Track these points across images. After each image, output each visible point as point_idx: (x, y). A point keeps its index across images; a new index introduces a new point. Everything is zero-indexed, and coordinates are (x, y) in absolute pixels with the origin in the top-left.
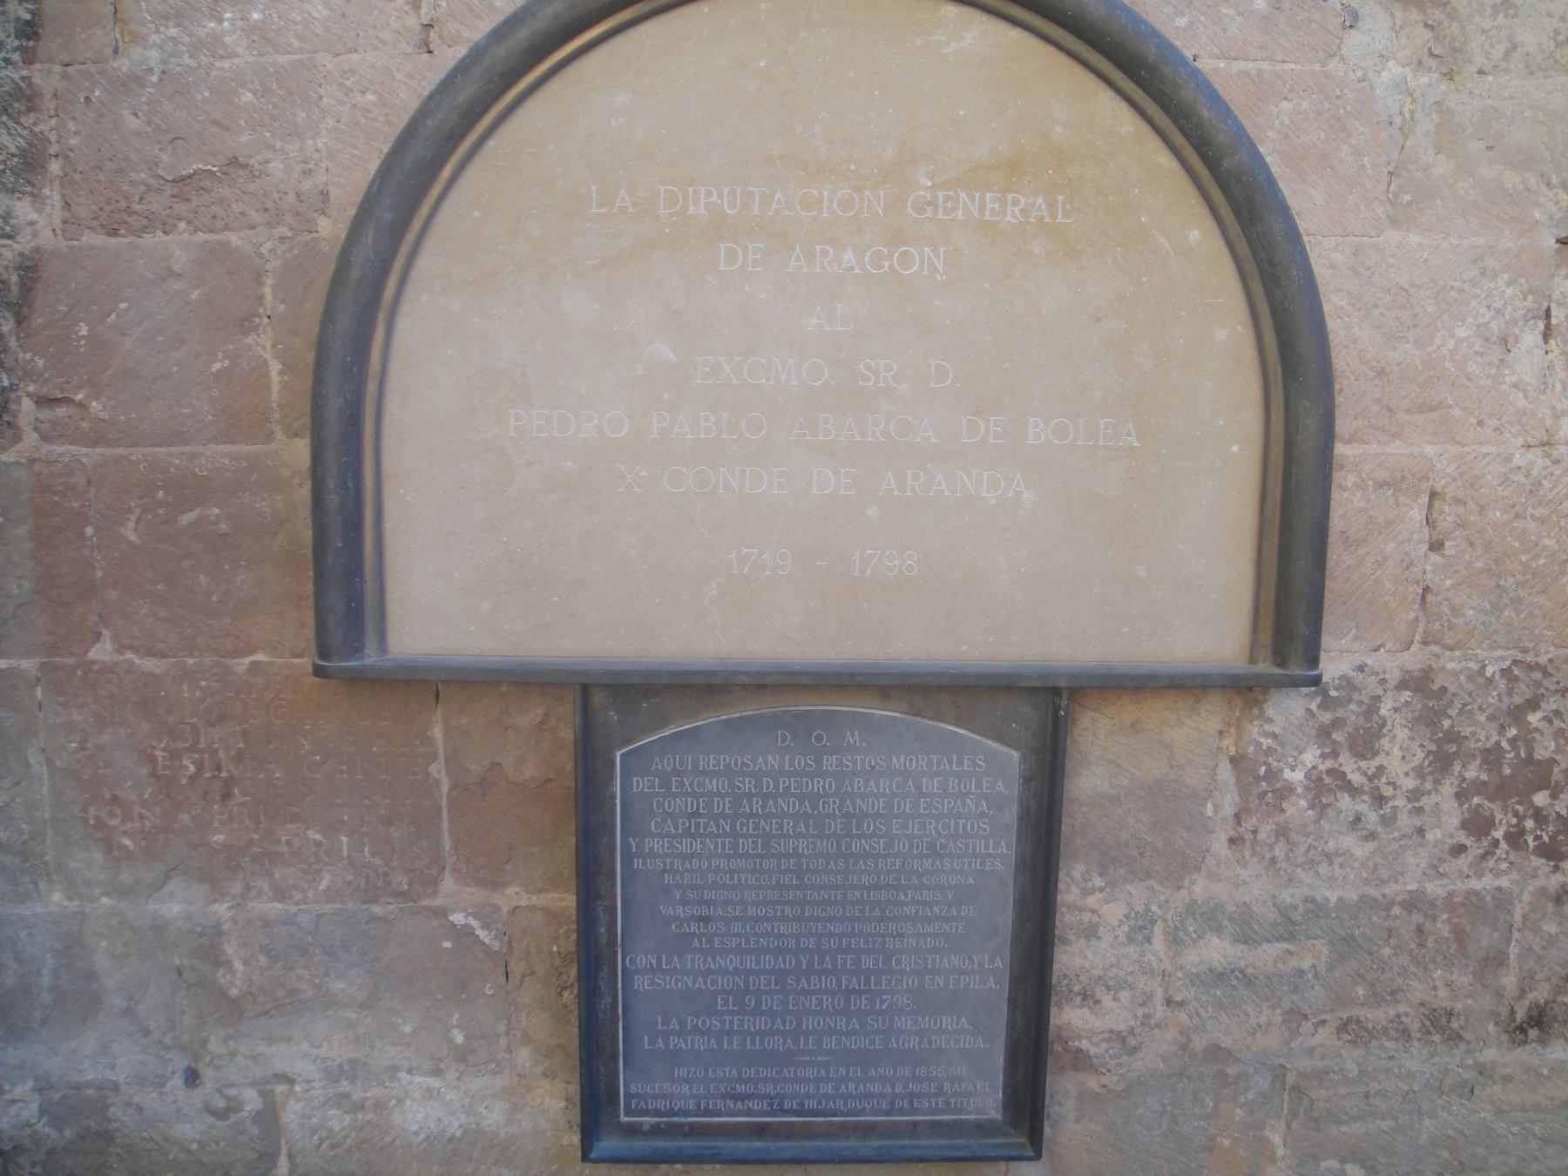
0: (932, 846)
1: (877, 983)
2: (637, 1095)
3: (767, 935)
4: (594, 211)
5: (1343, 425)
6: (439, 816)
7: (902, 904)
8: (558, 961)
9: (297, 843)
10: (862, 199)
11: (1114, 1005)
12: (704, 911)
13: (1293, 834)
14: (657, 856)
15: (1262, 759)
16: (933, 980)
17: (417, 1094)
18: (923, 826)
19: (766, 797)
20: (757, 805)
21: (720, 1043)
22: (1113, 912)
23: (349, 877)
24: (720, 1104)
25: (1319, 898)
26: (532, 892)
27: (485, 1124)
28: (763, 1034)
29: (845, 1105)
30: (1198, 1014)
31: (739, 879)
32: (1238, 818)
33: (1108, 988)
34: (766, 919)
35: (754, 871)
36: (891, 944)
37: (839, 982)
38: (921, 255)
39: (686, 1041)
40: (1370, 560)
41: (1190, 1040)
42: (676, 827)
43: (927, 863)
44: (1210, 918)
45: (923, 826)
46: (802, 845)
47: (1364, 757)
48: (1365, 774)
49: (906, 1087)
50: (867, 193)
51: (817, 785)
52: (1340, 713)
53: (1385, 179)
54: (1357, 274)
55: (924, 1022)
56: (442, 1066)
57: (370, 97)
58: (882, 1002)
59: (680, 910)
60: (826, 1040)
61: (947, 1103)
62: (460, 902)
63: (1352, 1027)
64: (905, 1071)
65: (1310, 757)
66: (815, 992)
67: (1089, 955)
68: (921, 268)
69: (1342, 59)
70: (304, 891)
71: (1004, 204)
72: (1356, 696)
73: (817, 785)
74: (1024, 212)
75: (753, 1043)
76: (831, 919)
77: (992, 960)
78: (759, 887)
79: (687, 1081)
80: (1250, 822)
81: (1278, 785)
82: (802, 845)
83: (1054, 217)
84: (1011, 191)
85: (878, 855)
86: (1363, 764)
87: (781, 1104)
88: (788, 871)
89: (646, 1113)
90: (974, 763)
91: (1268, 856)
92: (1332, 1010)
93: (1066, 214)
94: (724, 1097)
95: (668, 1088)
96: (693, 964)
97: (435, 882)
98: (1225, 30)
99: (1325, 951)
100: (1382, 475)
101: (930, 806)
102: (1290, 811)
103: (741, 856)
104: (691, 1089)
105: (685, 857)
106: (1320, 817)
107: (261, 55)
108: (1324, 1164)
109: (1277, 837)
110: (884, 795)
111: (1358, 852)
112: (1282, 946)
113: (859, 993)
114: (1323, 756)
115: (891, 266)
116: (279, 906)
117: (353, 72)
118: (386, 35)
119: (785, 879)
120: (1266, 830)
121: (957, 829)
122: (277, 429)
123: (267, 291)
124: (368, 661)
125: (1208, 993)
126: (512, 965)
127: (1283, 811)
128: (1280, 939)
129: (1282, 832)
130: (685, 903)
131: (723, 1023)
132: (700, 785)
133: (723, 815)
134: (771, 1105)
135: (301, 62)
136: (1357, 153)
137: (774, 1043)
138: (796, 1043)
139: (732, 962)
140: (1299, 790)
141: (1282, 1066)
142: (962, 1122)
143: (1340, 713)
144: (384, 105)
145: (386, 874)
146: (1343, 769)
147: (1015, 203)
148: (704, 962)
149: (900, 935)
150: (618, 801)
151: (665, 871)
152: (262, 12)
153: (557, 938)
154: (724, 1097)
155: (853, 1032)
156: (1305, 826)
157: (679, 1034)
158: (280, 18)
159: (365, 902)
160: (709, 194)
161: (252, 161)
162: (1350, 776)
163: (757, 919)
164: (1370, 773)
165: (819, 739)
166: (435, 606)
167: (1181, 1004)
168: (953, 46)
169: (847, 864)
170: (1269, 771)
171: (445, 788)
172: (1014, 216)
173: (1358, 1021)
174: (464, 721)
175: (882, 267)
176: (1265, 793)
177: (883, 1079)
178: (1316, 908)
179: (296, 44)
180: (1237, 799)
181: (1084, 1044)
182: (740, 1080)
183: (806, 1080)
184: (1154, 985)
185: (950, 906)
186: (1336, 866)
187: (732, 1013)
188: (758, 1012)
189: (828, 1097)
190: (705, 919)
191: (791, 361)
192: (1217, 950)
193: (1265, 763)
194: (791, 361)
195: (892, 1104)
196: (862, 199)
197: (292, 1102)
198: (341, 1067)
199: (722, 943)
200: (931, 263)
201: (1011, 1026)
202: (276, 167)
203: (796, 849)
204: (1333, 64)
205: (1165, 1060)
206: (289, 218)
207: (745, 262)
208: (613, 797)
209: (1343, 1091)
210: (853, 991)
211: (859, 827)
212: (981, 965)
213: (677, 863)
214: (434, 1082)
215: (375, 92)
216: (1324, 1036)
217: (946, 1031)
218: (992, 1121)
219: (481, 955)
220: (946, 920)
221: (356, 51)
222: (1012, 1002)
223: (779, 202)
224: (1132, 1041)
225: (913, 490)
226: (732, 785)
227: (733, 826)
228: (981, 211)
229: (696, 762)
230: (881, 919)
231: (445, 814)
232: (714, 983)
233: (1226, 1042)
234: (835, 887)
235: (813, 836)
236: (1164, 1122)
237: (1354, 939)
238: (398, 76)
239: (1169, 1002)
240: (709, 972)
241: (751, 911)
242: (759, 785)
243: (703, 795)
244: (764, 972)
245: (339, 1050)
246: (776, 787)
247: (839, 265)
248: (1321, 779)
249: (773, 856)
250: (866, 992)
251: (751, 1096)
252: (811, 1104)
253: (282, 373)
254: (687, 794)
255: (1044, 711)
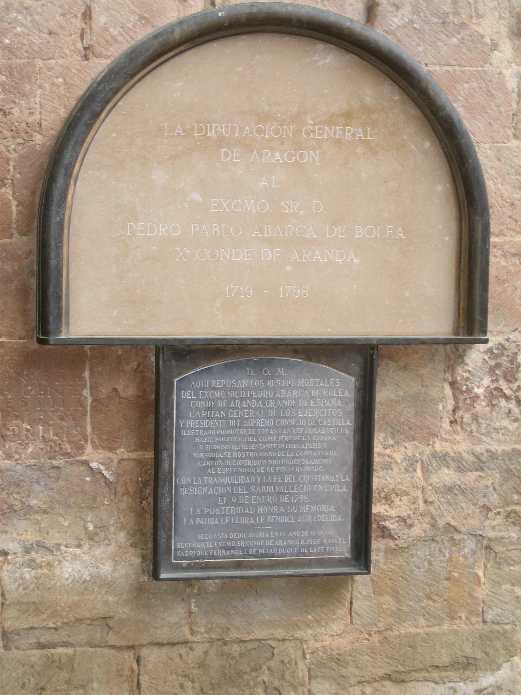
0: (316, 422)
1: (293, 489)
2: (180, 549)
3: (242, 466)
4: (166, 134)
5: (494, 228)
6: (86, 415)
7: (303, 450)
8: (141, 485)
9: (17, 429)
10: (283, 129)
11: (400, 503)
12: (213, 455)
13: (479, 418)
14: (192, 428)
15: (463, 383)
16: (318, 487)
17: (69, 558)
18: (312, 412)
19: (242, 400)
20: (238, 404)
21: (219, 521)
22: (398, 457)
23: (42, 446)
24: (219, 552)
25: (493, 450)
26: (129, 452)
27: (101, 572)
28: (240, 516)
29: (278, 551)
30: (439, 508)
31: (230, 439)
32: (454, 411)
33: (397, 495)
34: (242, 458)
35: (236, 435)
36: (298, 469)
37: (275, 489)
38: (309, 154)
39: (204, 520)
40: (509, 289)
41: (436, 521)
42: (201, 415)
43: (314, 430)
44: (443, 459)
45: (312, 412)
46: (258, 422)
47: (511, 382)
48: (512, 389)
49: (306, 542)
50: (285, 127)
51: (265, 394)
52: (499, 361)
53: (511, 117)
54: (499, 160)
55: (314, 509)
56: (82, 543)
57: (60, 80)
58: (295, 498)
59: (202, 455)
60: (269, 518)
61: (325, 549)
62: (95, 457)
63: (513, 515)
64: (305, 534)
65: (486, 381)
66: (263, 494)
67: (388, 478)
68: (309, 159)
69: (491, 64)
70: (20, 454)
71: (344, 131)
72: (505, 353)
73: (265, 394)
74: (353, 135)
75: (235, 521)
76: (271, 458)
77: (344, 477)
78: (238, 443)
79: (204, 541)
80: (459, 414)
81: (472, 395)
82: (258, 422)
83: (366, 137)
84: (347, 126)
85: (293, 427)
86: (511, 385)
87: (248, 552)
88: (250, 435)
89: (185, 558)
90: (335, 383)
91: (469, 429)
92: (503, 507)
93: (371, 136)
94: (221, 548)
95: (195, 545)
96: (208, 482)
97: (83, 448)
98: (439, 52)
99: (498, 476)
100: (513, 251)
101: (315, 403)
102: (478, 408)
103: (230, 428)
104: (205, 545)
105: (205, 429)
106: (492, 410)
107: (9, 59)
108: (504, 587)
109: (473, 420)
110: (295, 398)
111: (510, 427)
112: (477, 473)
113: (284, 494)
114: (492, 381)
115: (296, 159)
116: (7, 462)
117: (52, 69)
118: (67, 52)
119: (250, 439)
120: (467, 417)
121: (327, 413)
122: (15, 231)
123: (11, 168)
124: (63, 337)
125: (444, 497)
126: (118, 489)
127: (475, 407)
128: (477, 470)
129: (475, 417)
130: (204, 451)
131: (221, 510)
132: (213, 394)
133: (222, 409)
134: (243, 552)
135: (28, 63)
136: (498, 106)
137: (245, 520)
138: (255, 520)
139: (225, 480)
140: (482, 398)
141: (481, 535)
142: (332, 559)
143: (499, 361)
144: (67, 84)
145: (60, 444)
146: (501, 387)
147: (349, 131)
148: (213, 480)
149: (302, 465)
150: (175, 403)
151: (196, 436)
152: (10, 39)
153: (141, 473)
154: (221, 548)
155: (281, 514)
156: (485, 415)
157: (200, 517)
158: (19, 42)
159: (49, 459)
160: (217, 127)
161: (5, 108)
162: (505, 391)
163: (237, 459)
164: (514, 389)
165: (266, 372)
166: (92, 312)
167: (432, 503)
168: (322, 62)
169: (278, 431)
170: (468, 389)
171: (89, 401)
172: (349, 137)
173: (515, 512)
174: (101, 368)
175: (292, 160)
176: (465, 399)
177: (295, 538)
178: (493, 455)
179: (26, 55)
180: (453, 402)
181: (387, 524)
182: (229, 540)
183: (260, 539)
184: (419, 494)
185: (325, 451)
186: (500, 435)
187: (225, 505)
188: (237, 505)
189: (270, 547)
190: (213, 459)
191: (252, 201)
192: (447, 476)
193: (466, 385)
194: (252, 201)
195: (299, 550)
196: (283, 129)
197: (6, 565)
198: (32, 545)
199: (221, 471)
200: (313, 158)
201: (354, 508)
202: (16, 111)
203: (255, 424)
204: (487, 67)
205: (425, 532)
206: (23, 135)
207: (232, 157)
208: (173, 401)
209: (511, 548)
210: (281, 493)
211: (284, 413)
212: (339, 479)
213: (201, 432)
214: (78, 551)
215: (63, 78)
216: (499, 520)
217: (324, 513)
218: (346, 558)
219: (103, 484)
220: (323, 457)
221: (53, 58)
222: (354, 498)
223: (247, 131)
224: (409, 522)
225: (306, 259)
226: (227, 394)
227: (227, 414)
228: (335, 134)
229: (210, 384)
230: (294, 458)
231: (89, 414)
232: (217, 491)
233: (453, 523)
234: (273, 442)
235: (263, 418)
236: (426, 564)
237: (511, 471)
238: (74, 71)
239: (425, 502)
240: (216, 485)
241: (235, 455)
242: (238, 394)
243: (214, 399)
244: (240, 484)
245: (31, 537)
246: (246, 395)
247: (273, 159)
248: (491, 393)
249: (245, 428)
250: (287, 494)
251: (233, 548)
252: (262, 551)
253: (17, 206)
254: (206, 399)
255: (364, 360)
